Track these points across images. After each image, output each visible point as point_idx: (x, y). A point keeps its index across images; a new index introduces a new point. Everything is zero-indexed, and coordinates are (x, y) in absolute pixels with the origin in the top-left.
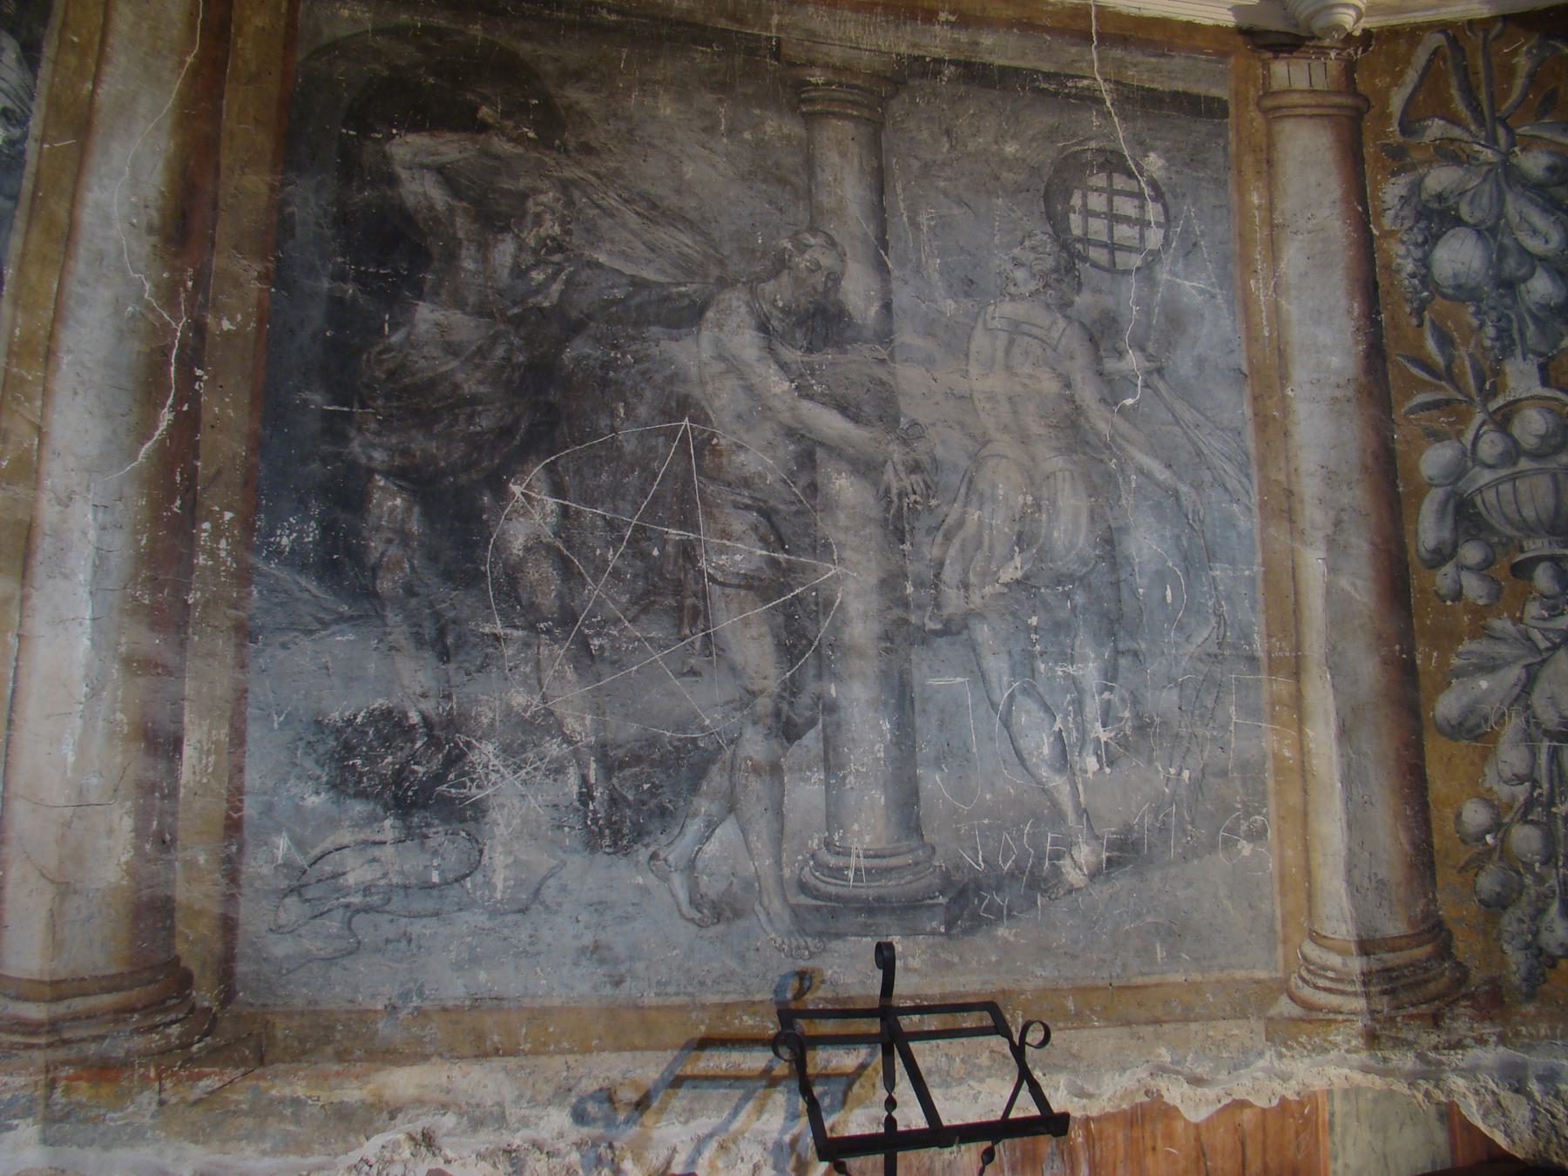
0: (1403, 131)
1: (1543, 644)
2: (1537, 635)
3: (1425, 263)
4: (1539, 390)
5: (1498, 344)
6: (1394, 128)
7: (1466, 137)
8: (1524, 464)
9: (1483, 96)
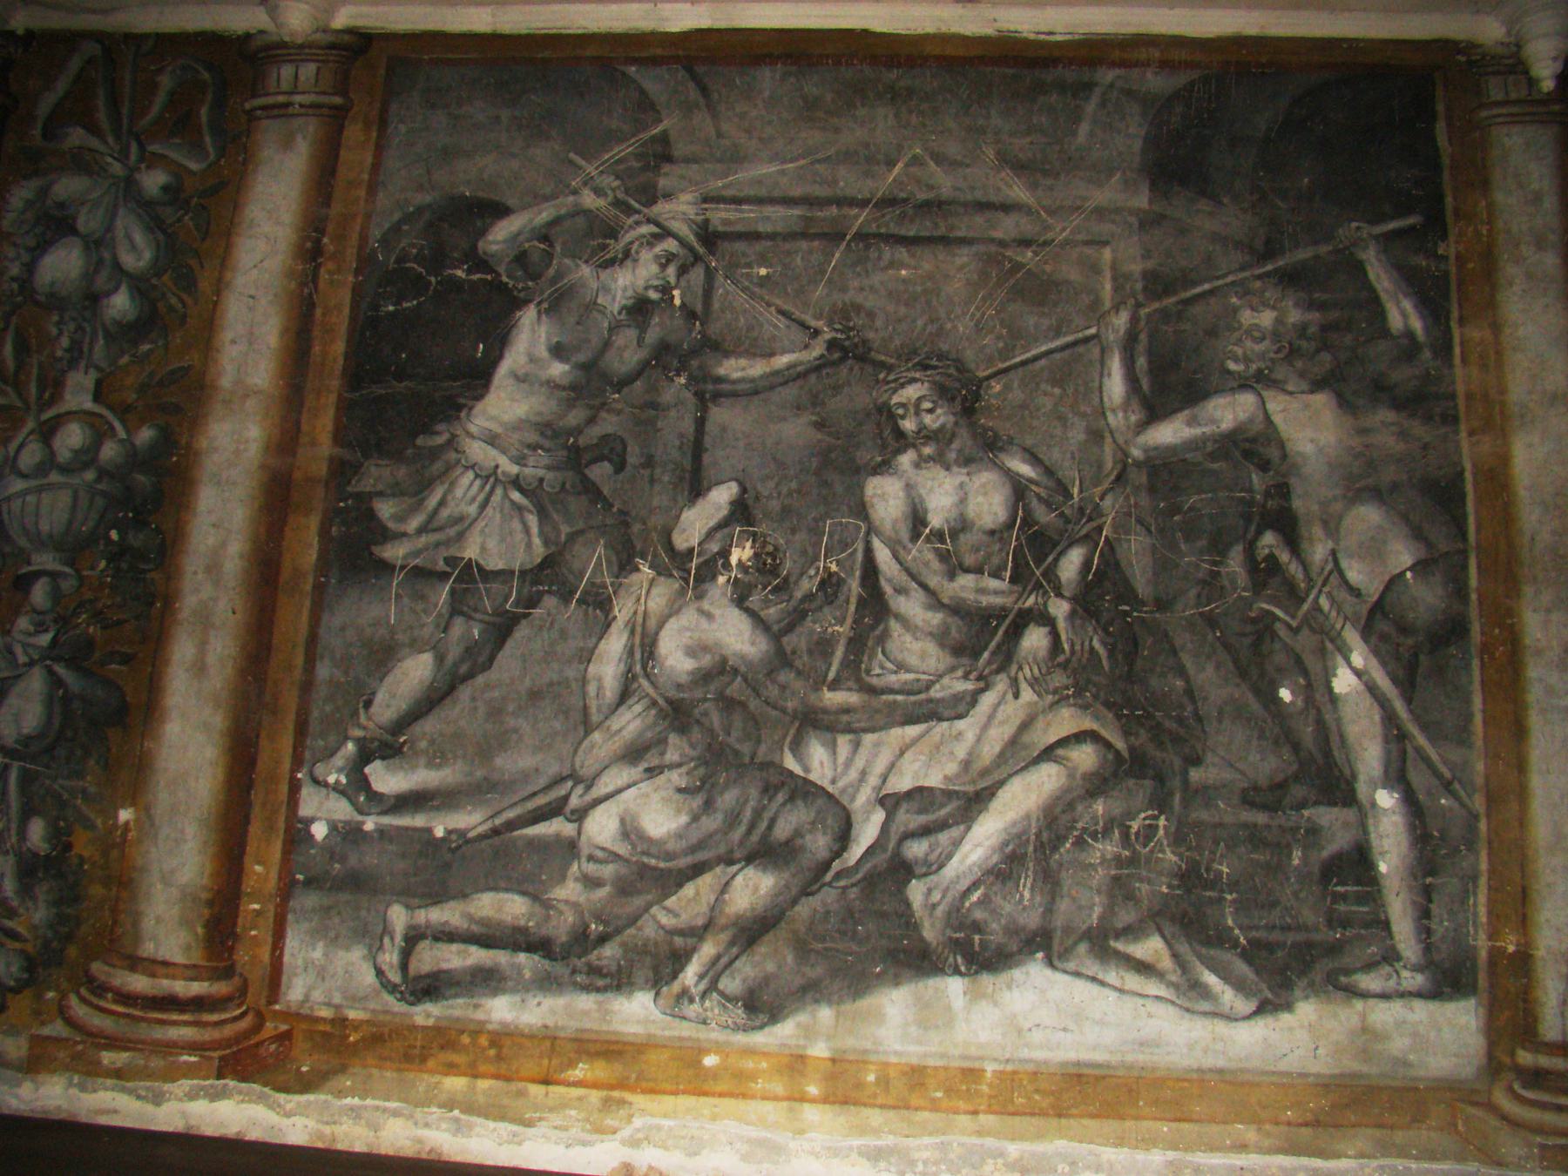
0: (44, 136)
1: (22, 659)
2: (18, 650)
3: (31, 267)
4: (89, 405)
5: (68, 356)
6: (37, 132)
7: (102, 148)
8: (55, 477)
9: (125, 111)
